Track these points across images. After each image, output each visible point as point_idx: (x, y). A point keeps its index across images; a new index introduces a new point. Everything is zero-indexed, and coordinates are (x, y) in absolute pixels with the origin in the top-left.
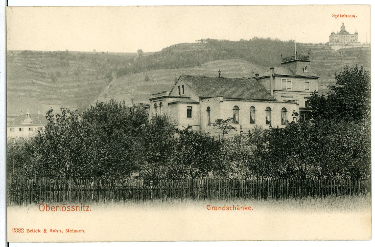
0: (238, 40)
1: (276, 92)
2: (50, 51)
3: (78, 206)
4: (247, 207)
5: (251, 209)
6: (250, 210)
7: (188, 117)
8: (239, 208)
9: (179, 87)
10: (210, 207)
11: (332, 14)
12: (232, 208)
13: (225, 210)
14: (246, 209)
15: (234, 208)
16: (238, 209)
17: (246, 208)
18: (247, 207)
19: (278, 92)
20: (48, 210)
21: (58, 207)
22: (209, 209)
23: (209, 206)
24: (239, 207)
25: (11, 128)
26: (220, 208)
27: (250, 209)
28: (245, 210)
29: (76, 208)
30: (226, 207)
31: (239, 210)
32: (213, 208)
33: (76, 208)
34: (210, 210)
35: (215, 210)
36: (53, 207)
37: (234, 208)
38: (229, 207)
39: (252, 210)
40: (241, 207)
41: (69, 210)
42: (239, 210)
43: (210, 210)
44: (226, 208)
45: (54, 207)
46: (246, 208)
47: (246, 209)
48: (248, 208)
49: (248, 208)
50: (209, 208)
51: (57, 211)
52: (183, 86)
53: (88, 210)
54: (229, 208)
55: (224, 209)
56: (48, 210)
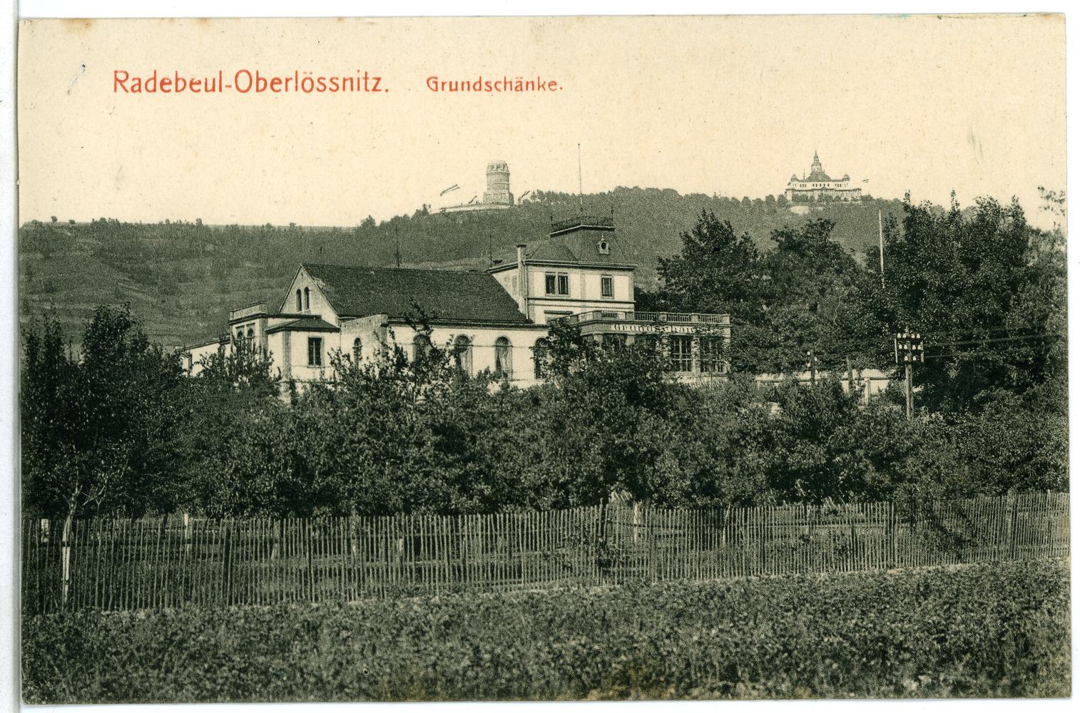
1: (531, 301)
5: (558, 87)
7: (311, 362)
8: (139, 84)
9: (299, 292)
10: (436, 83)
11: (1011, 196)
12: (501, 86)
15: (508, 85)
16: (136, 88)
19: (537, 302)
20: (179, 88)
25: (556, 272)
26: (348, 84)
30: (483, 83)
32: (290, 83)
35: (451, 90)
37: (508, 85)
43: (437, 89)
44: (484, 86)
46: (541, 83)
49: (546, 86)
50: (433, 86)
51: (287, 90)
52: (307, 290)
54: (493, 85)
55: (477, 86)
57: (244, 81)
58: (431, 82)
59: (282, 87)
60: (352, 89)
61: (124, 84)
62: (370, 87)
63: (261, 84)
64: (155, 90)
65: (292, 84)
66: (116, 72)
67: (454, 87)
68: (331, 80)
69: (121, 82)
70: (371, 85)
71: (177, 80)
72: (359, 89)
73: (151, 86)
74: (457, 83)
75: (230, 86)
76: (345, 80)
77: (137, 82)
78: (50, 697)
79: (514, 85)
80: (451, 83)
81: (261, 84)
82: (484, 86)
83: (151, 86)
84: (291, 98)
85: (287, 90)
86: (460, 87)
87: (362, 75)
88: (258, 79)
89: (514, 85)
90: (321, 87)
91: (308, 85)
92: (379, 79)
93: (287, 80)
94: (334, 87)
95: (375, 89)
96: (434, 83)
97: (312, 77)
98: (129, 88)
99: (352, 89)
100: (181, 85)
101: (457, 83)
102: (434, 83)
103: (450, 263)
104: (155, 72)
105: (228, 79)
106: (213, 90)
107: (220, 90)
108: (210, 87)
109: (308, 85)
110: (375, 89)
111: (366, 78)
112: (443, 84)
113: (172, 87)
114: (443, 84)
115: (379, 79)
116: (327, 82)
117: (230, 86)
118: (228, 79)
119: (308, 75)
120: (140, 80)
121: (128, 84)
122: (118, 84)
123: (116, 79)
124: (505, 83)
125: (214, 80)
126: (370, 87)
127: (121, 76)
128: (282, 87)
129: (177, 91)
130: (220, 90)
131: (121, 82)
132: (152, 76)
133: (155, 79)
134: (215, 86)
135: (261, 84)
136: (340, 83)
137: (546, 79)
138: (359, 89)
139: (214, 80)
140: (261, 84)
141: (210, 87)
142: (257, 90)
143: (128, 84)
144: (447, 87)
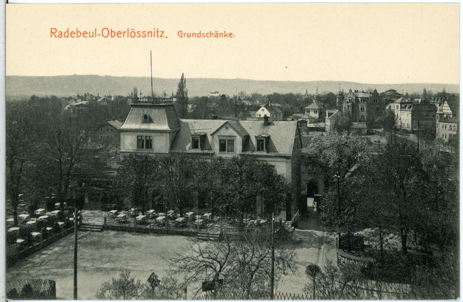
0: (72, 74)
2: (106, 76)
3: (150, 32)
4: (227, 34)
5: (233, 36)
6: (232, 37)
8: (61, 34)
10: (182, 34)
12: (209, 35)
13: (200, 37)
14: (226, 36)
15: (212, 35)
16: (216, 36)
17: (226, 35)
18: (227, 34)
21: (126, 32)
22: (181, 36)
23: (181, 32)
24: (217, 34)
27: (231, 36)
28: (225, 37)
29: (148, 34)
31: (61, 37)
33: (148, 34)
34: (182, 37)
35: (188, 37)
36: (72, 33)
38: (206, 34)
39: (234, 36)
40: (220, 34)
41: (144, 35)
42: (61, 37)
43: (182, 37)
45: (73, 33)
46: (226, 34)
47: (226, 36)
48: (228, 35)
49: (228, 35)
50: (181, 35)
51: (124, 37)
53: (162, 36)
56: (113, 35)
57: (105, 33)
58: (180, 33)
59: (122, 35)
60: (152, 37)
61: (55, 34)
62: (159, 35)
63: (112, 34)
64: (68, 37)
65: (126, 34)
66: (51, 29)
67: (189, 35)
68: (137, 32)
69: (53, 33)
70: (160, 34)
71: (77, 32)
72: (154, 36)
73: (66, 35)
74: (190, 34)
75: (99, 35)
76: (148, 32)
77: (60, 33)
78: (456, 282)
79: (214, 35)
80: (188, 34)
81: (113, 34)
82: (202, 35)
83: (66, 35)
84: (126, 40)
85: (124, 37)
86: (192, 35)
87: (156, 30)
88: (112, 32)
89: (214, 35)
90: (139, 36)
91: (133, 35)
92: (163, 32)
93: (124, 32)
94: (144, 35)
95: (161, 36)
96: (181, 34)
97: (135, 31)
98: (57, 36)
99: (152, 37)
100: (79, 34)
101: (190, 34)
102: (181, 34)
103: (249, 152)
104: (200, 32)
105: (99, 32)
106: (93, 36)
107: (96, 37)
108: (91, 35)
109: (133, 35)
110: (161, 36)
111: (158, 32)
112: (185, 34)
113: (75, 35)
114: (185, 34)
115: (163, 32)
116: (142, 34)
117: (99, 35)
118: (99, 32)
119: (133, 30)
120: (61, 32)
121: (57, 34)
122: (52, 34)
123: (51, 32)
124: (211, 34)
125: (93, 32)
126: (159, 35)
127: (54, 31)
128: (122, 35)
129: (77, 37)
130: (96, 37)
131: (53, 33)
132: (67, 31)
133: (68, 32)
134: (94, 35)
135: (113, 34)
136: (146, 33)
137: (228, 32)
138: (154, 36)
139: (93, 32)
140: (112, 34)
141: (91, 35)
142: (112, 37)
143: (57, 34)
144: (186, 35)
